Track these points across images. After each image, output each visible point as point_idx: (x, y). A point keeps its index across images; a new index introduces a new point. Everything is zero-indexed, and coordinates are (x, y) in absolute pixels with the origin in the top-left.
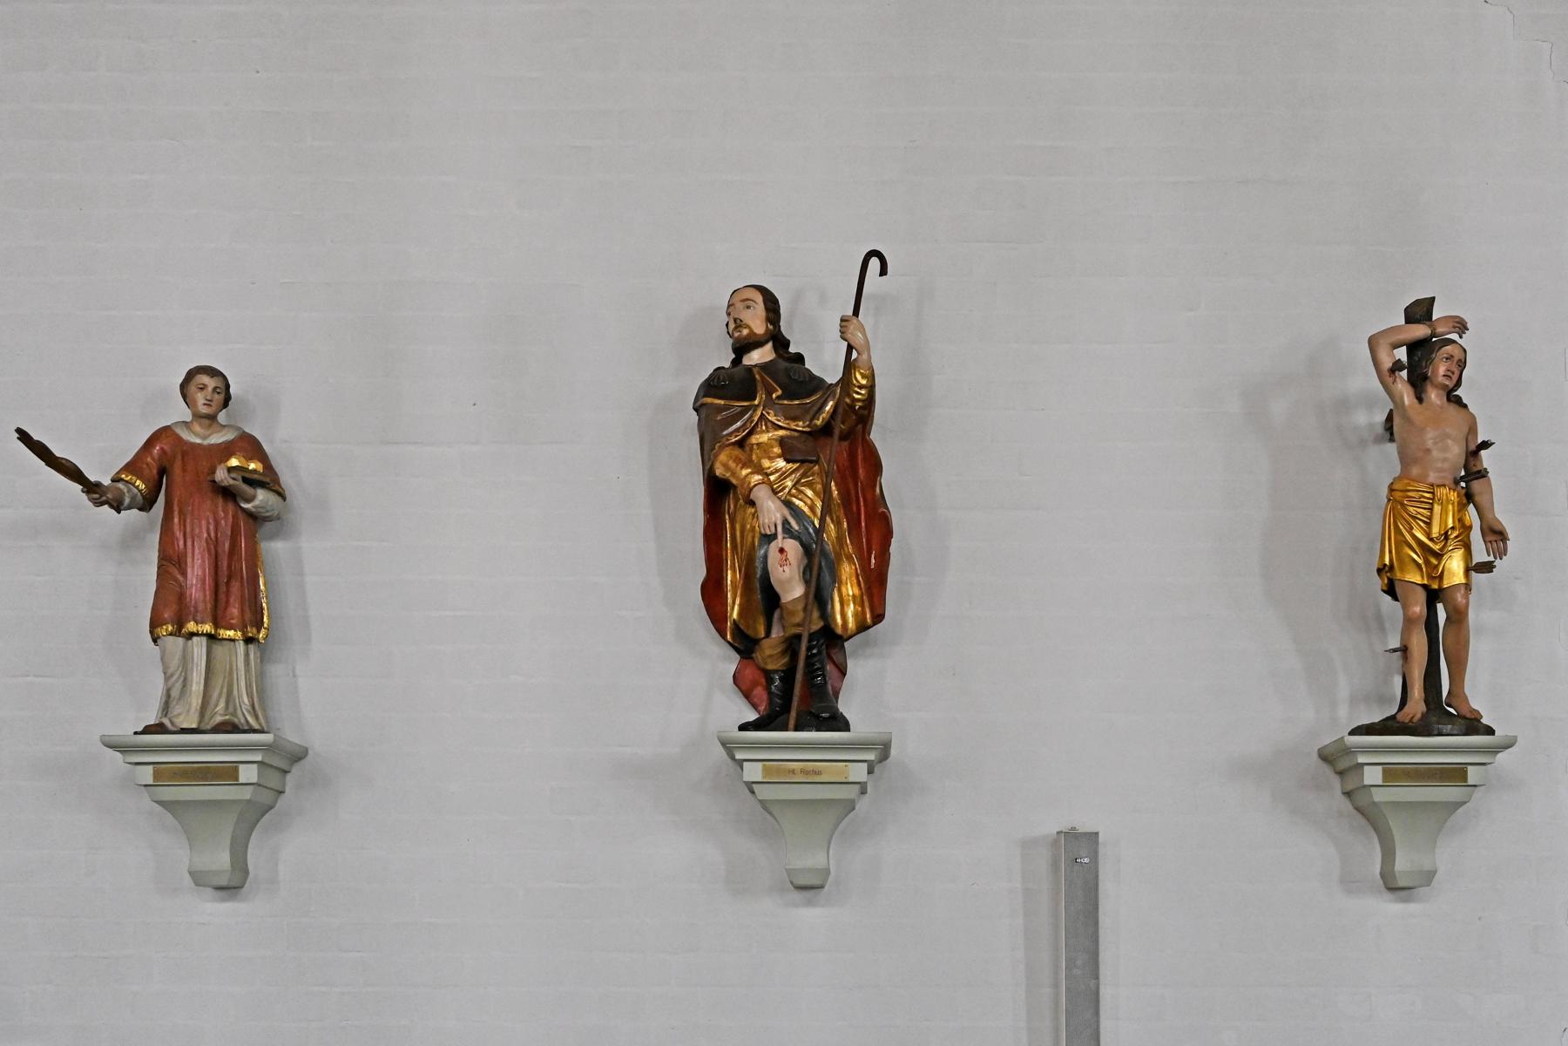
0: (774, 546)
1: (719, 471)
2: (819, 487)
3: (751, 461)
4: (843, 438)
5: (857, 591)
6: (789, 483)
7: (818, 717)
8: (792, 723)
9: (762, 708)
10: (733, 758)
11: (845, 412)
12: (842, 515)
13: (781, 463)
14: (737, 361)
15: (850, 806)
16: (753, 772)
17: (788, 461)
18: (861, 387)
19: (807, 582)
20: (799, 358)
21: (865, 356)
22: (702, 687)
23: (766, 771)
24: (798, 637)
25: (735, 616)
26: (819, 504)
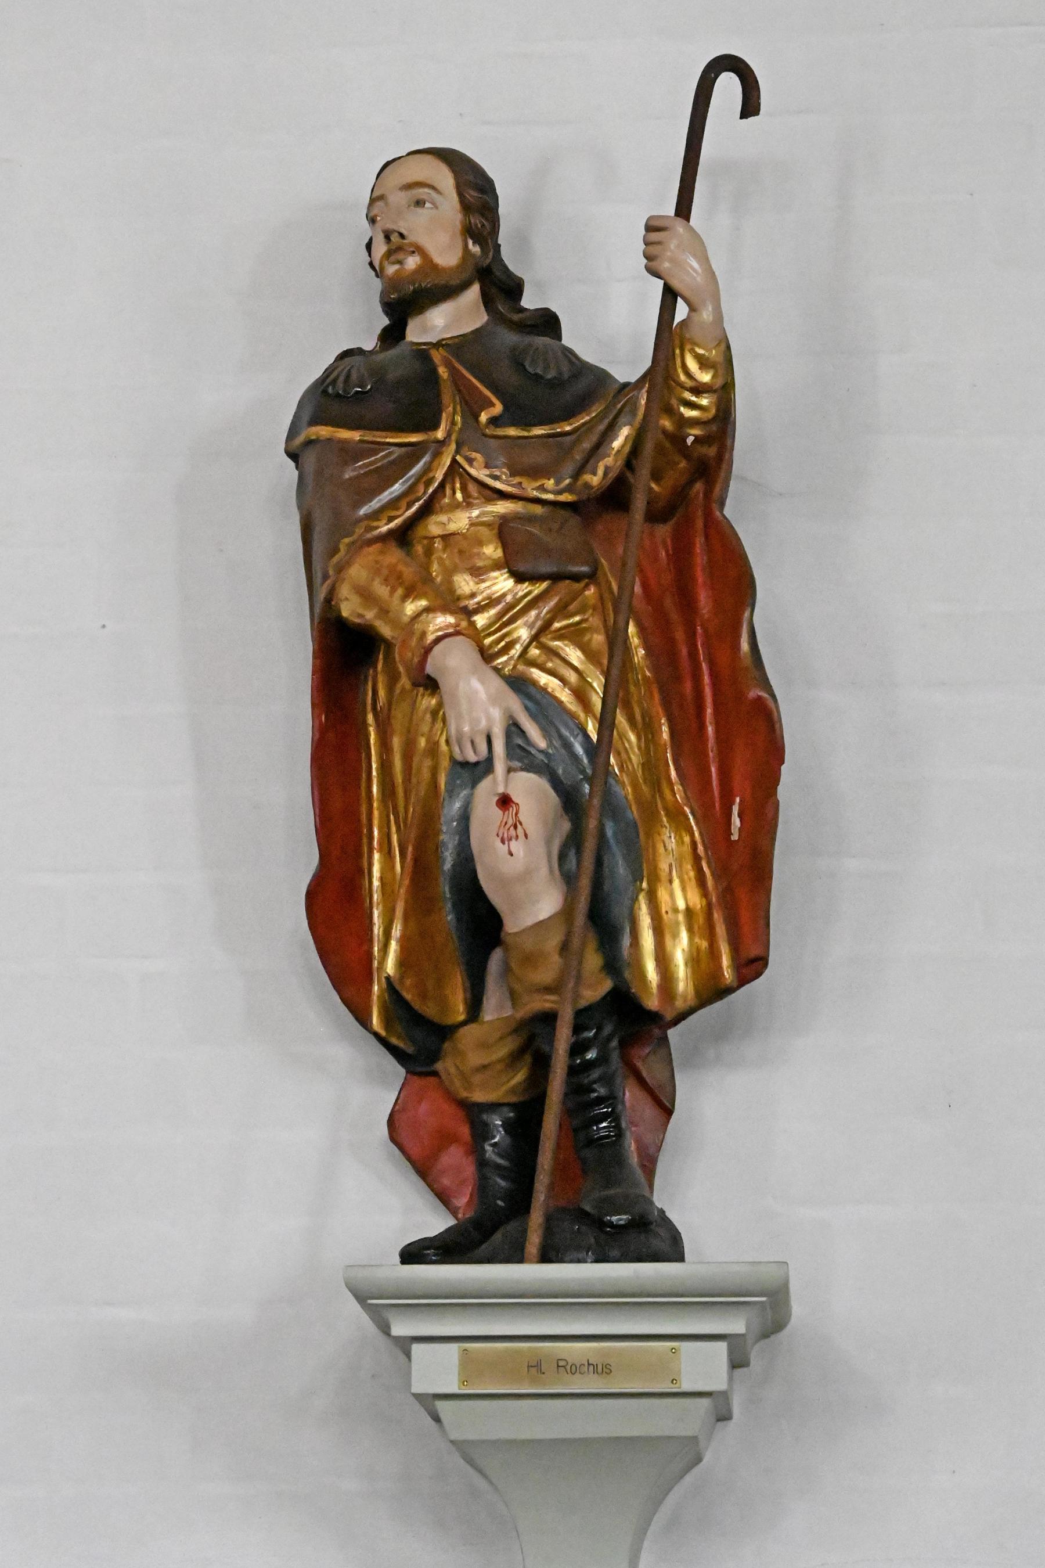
0: (486, 791)
1: (349, 608)
2: (598, 639)
3: (427, 579)
4: (655, 516)
5: (696, 900)
6: (523, 633)
7: (600, 1224)
8: (534, 1241)
9: (461, 1201)
10: (385, 1329)
11: (659, 449)
12: (658, 709)
13: (502, 583)
14: (393, 335)
15: (689, 1453)
16: (437, 1369)
17: (520, 578)
18: (699, 390)
19: (569, 880)
20: (548, 323)
21: (706, 315)
22: (300, 1154)
23: (469, 1367)
24: (549, 1019)
25: (390, 966)
26: (597, 683)
